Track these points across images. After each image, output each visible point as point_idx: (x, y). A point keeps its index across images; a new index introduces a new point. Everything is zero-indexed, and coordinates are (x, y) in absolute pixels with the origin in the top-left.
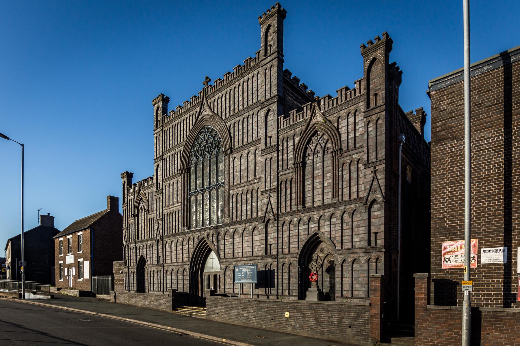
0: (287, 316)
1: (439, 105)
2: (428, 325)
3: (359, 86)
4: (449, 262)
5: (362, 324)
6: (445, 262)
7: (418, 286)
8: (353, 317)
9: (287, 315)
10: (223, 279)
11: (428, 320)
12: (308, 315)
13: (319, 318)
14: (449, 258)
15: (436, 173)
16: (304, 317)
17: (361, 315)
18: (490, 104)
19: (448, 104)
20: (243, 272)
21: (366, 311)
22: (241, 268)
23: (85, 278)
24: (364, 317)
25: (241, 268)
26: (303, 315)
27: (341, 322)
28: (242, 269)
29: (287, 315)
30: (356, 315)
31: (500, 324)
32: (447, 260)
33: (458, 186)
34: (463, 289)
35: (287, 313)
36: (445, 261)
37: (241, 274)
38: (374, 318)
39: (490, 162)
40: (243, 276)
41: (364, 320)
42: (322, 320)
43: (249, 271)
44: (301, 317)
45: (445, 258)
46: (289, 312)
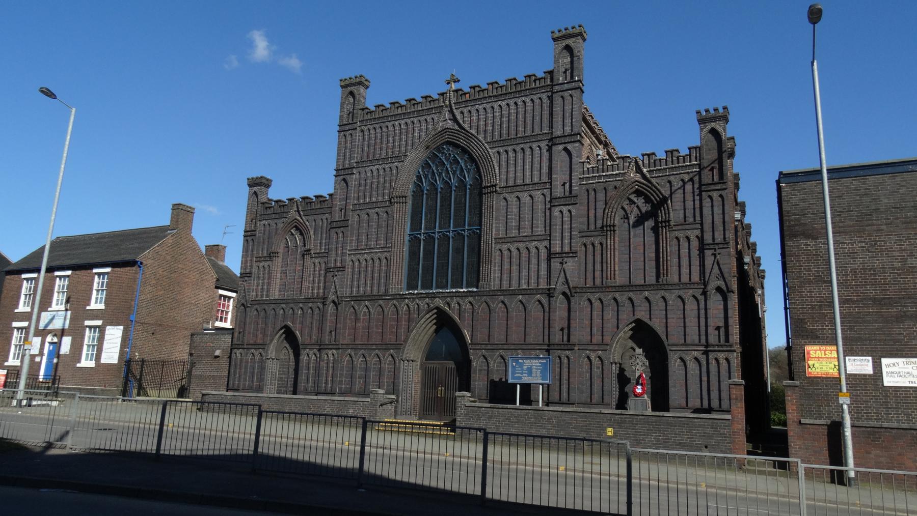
0: (610, 434)
1: (790, 198)
2: (804, 443)
3: (654, 270)
4: (814, 369)
5: (722, 443)
6: (810, 369)
7: (789, 396)
8: (709, 433)
9: (610, 432)
10: (718, 328)
11: (803, 437)
12: (644, 432)
13: (660, 436)
14: (814, 365)
15: (792, 269)
16: (637, 435)
17: (720, 431)
18: (841, 209)
19: (800, 200)
20: (525, 368)
21: (726, 426)
22: (522, 361)
23: (103, 361)
24: (724, 434)
25: (522, 361)
26: (636, 432)
27: (693, 441)
28: (524, 363)
29: (610, 432)
30: (714, 431)
31: (879, 441)
32: (812, 367)
33: (816, 286)
34: (841, 402)
35: (610, 429)
36: (810, 367)
37: (522, 370)
38: (738, 435)
39: (846, 267)
40: (525, 373)
41: (725, 437)
42: (666, 439)
43: (537, 366)
44: (632, 434)
45: (808, 365)
46: (614, 428)
